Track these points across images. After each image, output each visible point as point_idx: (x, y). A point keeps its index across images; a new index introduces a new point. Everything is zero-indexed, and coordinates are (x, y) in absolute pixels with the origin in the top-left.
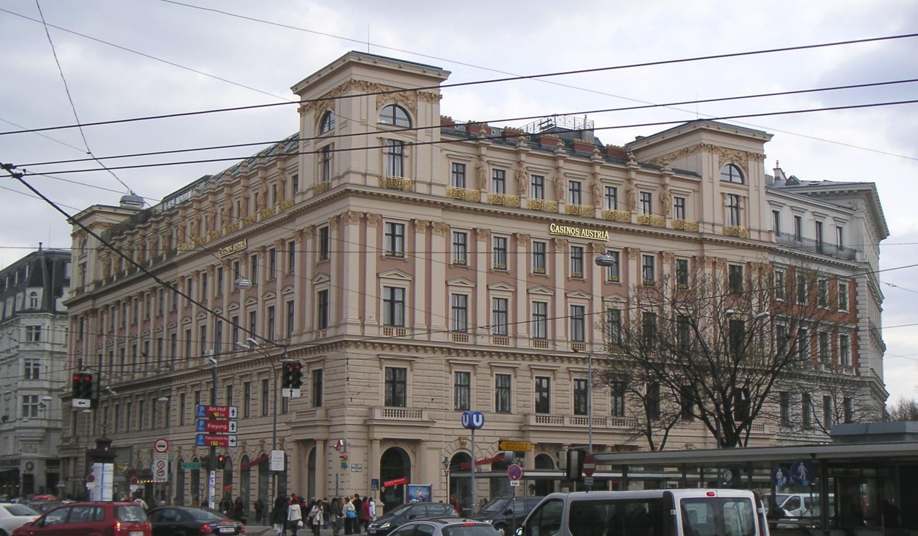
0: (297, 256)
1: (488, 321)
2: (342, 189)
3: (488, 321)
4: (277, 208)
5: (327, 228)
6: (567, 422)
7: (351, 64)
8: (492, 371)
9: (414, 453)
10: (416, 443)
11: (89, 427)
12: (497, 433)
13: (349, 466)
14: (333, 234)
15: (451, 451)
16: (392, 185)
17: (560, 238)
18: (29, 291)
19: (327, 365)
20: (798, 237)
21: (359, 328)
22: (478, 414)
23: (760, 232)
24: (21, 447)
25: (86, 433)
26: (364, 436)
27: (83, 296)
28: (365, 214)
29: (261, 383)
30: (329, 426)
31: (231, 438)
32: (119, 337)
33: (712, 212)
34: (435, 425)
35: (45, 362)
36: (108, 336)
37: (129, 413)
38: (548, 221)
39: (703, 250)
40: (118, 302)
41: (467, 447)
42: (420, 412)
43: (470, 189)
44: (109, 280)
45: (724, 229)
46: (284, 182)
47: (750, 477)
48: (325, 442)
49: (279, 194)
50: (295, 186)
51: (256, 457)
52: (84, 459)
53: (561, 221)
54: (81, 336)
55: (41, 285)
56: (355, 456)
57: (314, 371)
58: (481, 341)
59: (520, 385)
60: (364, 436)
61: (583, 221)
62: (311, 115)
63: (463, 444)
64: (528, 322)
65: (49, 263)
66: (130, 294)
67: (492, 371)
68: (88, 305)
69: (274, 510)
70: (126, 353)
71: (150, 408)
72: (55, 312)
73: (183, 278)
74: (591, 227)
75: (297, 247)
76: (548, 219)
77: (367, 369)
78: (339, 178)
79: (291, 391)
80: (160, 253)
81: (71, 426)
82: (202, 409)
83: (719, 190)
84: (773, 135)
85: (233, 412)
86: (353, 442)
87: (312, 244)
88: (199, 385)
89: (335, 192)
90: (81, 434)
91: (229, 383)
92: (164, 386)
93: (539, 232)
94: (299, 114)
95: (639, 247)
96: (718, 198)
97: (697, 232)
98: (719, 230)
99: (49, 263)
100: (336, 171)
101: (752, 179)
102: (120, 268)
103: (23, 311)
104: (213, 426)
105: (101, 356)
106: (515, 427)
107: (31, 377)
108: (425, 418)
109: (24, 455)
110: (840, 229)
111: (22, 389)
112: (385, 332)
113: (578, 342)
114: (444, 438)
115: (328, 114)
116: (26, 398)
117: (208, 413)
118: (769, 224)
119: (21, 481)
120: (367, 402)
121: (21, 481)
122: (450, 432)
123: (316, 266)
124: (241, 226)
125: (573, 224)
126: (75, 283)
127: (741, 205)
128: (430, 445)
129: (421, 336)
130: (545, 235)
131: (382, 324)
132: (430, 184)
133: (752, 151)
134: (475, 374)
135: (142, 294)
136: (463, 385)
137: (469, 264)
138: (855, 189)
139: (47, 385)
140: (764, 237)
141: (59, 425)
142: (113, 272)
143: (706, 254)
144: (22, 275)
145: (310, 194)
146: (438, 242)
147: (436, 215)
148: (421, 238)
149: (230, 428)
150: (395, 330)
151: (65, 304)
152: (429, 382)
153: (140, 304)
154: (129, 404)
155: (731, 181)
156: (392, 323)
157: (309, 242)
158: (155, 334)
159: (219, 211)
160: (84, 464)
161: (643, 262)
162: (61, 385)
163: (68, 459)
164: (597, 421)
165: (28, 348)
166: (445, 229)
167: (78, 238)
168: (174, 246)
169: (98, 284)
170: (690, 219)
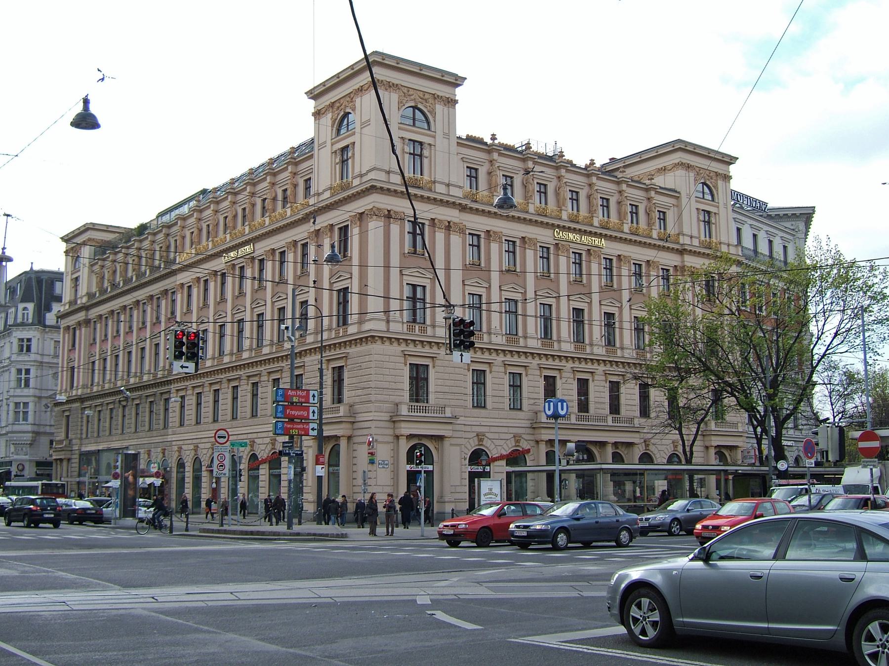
1: (536, 312)
3: (536, 312)
6: (573, 421)
10: (440, 438)
11: (82, 430)
13: (376, 462)
14: (354, 233)
15: (469, 447)
17: (563, 243)
18: (21, 306)
19: (349, 362)
20: (755, 251)
21: (384, 323)
22: (562, 401)
23: (729, 245)
24: (12, 449)
26: (390, 432)
27: (77, 307)
29: (230, 390)
37: (124, 416)
39: (683, 261)
41: (484, 443)
42: (443, 409)
44: (103, 291)
46: (295, 186)
49: (249, 216)
50: (307, 188)
51: (265, 456)
52: (77, 460)
53: (564, 227)
56: (383, 452)
59: (532, 384)
60: (390, 432)
61: (583, 228)
62: (327, 119)
66: (139, 298)
68: (81, 316)
70: (97, 367)
71: (147, 410)
72: (45, 326)
74: (590, 233)
76: (553, 224)
77: (391, 365)
78: (361, 176)
79: (462, 355)
80: (143, 268)
81: (63, 430)
82: (280, 392)
86: (380, 439)
90: (73, 436)
91: (216, 387)
92: (164, 389)
93: (545, 236)
95: (630, 254)
96: (694, 212)
97: (678, 243)
101: (721, 196)
103: (16, 325)
104: (293, 413)
105: (94, 363)
106: (527, 423)
108: (448, 414)
109: (16, 457)
116: (17, 404)
117: (286, 398)
120: (392, 398)
122: (190, 442)
124: (210, 247)
125: (574, 230)
126: (67, 298)
127: (713, 220)
128: (453, 441)
131: (405, 321)
132: (448, 185)
136: (479, 379)
137: (483, 265)
138: (798, 212)
143: (686, 263)
147: (453, 215)
149: (311, 415)
150: (417, 327)
153: (98, 326)
156: (414, 321)
159: (158, 249)
160: (77, 465)
163: (61, 460)
165: (20, 358)
169: (90, 295)
170: (671, 229)
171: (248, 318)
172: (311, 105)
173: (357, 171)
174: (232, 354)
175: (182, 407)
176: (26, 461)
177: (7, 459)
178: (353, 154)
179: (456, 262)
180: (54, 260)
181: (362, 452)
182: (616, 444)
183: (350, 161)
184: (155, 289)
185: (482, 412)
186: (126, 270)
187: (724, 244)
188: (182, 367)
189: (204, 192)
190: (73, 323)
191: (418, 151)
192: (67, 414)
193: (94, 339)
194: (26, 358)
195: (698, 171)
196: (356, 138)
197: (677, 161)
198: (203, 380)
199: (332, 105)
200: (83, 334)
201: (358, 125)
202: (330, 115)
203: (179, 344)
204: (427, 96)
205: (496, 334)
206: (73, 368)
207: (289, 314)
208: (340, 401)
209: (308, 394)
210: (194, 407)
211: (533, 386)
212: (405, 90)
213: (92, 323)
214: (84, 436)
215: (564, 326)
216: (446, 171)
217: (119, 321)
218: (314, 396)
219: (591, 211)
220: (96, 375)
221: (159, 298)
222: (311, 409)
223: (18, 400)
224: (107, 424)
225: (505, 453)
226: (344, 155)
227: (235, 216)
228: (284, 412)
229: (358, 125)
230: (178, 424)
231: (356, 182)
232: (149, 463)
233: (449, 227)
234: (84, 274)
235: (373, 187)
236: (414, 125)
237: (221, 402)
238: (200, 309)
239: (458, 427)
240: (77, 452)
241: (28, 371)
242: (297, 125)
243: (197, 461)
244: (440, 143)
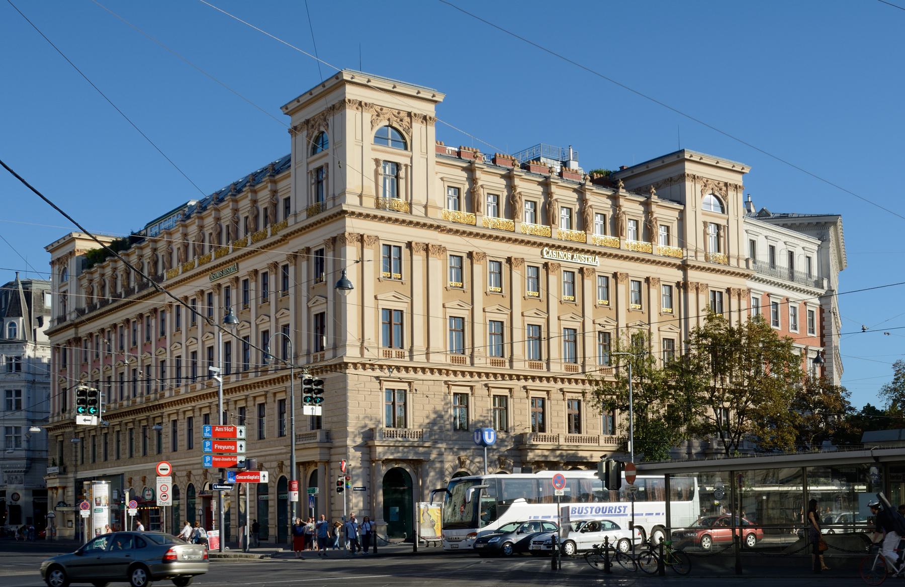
11: (76, 456)
14: (329, 257)
25: (74, 463)
27: (65, 324)
37: (118, 441)
40: (103, 330)
44: (92, 308)
47: (805, 488)
49: (270, 217)
50: (287, 208)
54: (65, 366)
62: (302, 136)
68: (70, 334)
69: (565, 570)
71: (141, 435)
87: (305, 268)
92: (156, 413)
94: (289, 135)
104: (220, 447)
107: (13, 407)
110: (809, 258)
119: (8, 513)
121: (8, 513)
129: (420, 359)
135: (115, 326)
151: (46, 333)
157: (304, 264)
164: (590, 440)
167: (57, 267)
168: (160, 273)
171: (154, 364)
172: (49, 257)
175: (175, 432)
178: (327, 176)
183: (324, 182)
193: (86, 360)
194: (16, 377)
199: (307, 122)
202: (305, 133)
206: (65, 390)
213: (83, 342)
214: (79, 462)
221: (148, 317)
222: (239, 443)
224: (102, 450)
237: (194, 430)
240: (72, 480)
243: (191, 488)
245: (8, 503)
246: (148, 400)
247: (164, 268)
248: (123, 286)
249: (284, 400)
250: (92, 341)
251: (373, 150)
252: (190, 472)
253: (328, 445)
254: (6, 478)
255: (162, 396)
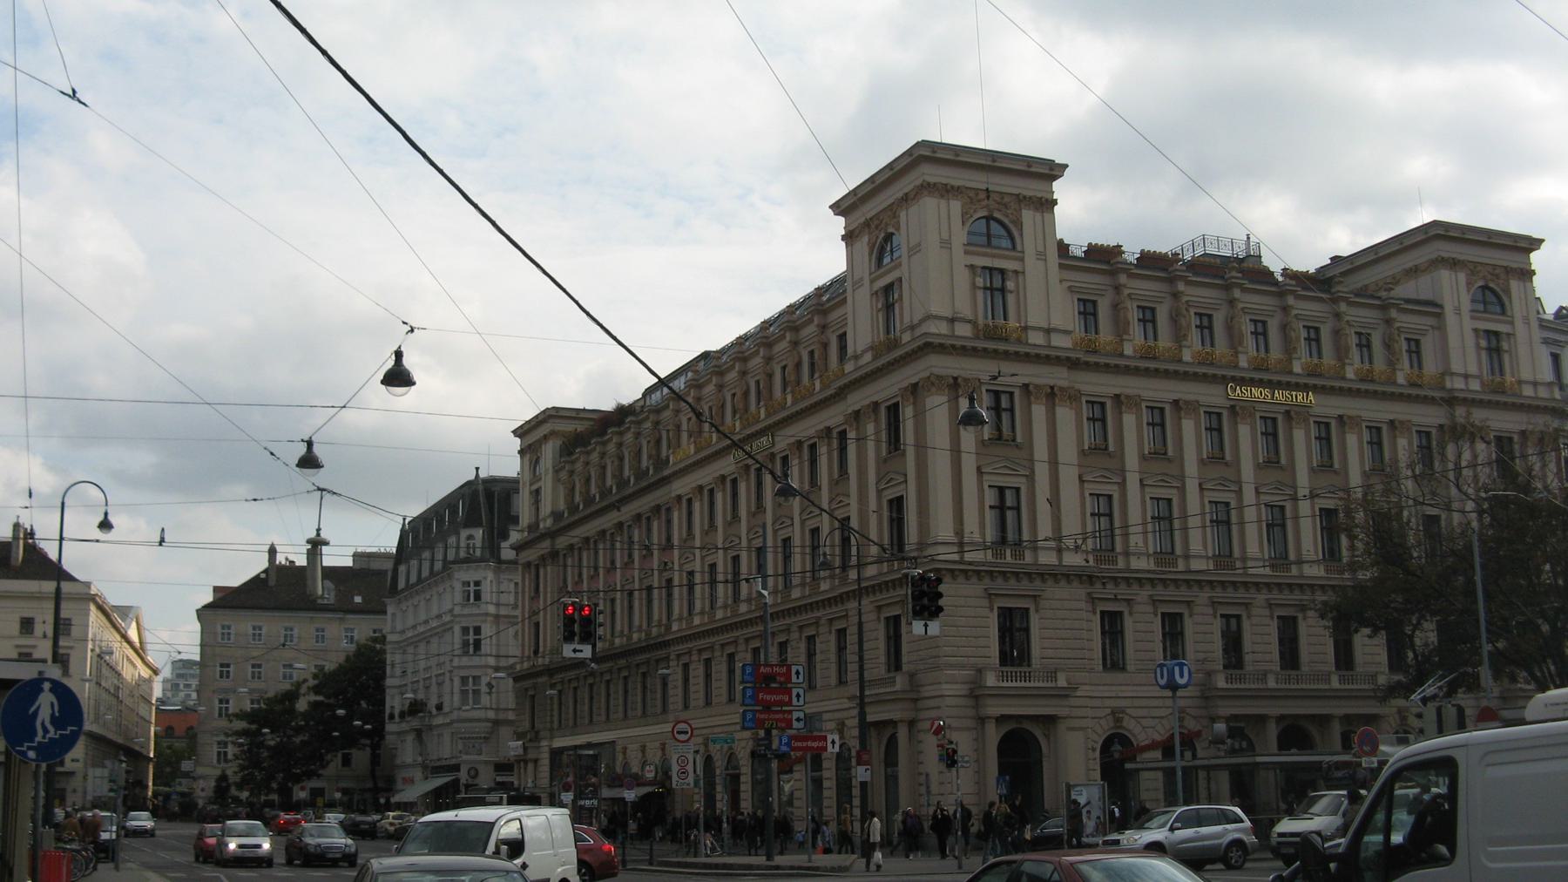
0: (852, 449)
2: (920, 343)
4: (763, 411)
5: (896, 405)
6: (1272, 684)
7: (551, 416)
8: (1156, 608)
9: (1047, 736)
10: (1050, 721)
12: (1108, 703)
14: (908, 412)
15: (1100, 731)
16: (992, 334)
18: (464, 533)
26: (971, 712)
28: (955, 379)
30: (916, 700)
31: (795, 715)
32: (641, 569)
33: (1462, 355)
34: (1079, 693)
35: (487, 630)
36: (680, 548)
37: (608, 695)
38: (1224, 380)
42: (1052, 675)
43: (1106, 335)
44: (573, 509)
45: (1482, 384)
46: (825, 346)
48: (912, 723)
49: (764, 392)
50: (843, 348)
55: (480, 525)
57: (887, 619)
58: (1136, 563)
60: (971, 712)
61: (1275, 378)
62: (863, 243)
63: (1118, 720)
64: (1204, 527)
65: (489, 495)
67: (1156, 608)
72: (500, 561)
73: (679, 498)
74: (1288, 386)
75: (851, 435)
76: (1224, 377)
78: (912, 328)
81: (527, 717)
83: (1468, 325)
84: (1542, 241)
85: (798, 673)
86: (954, 723)
88: (711, 648)
89: (908, 349)
91: (730, 650)
92: (661, 653)
93: (1210, 396)
98: (1475, 385)
99: (489, 495)
100: (907, 320)
102: (588, 491)
109: (465, 757)
111: (459, 667)
112: (995, 555)
113: (1280, 560)
114: (1090, 713)
115: (889, 237)
116: (464, 680)
118: (1547, 375)
122: (1097, 703)
123: (882, 462)
125: (1260, 383)
126: (525, 518)
129: (1047, 558)
130: (1220, 401)
133: (1515, 265)
134: (1131, 614)
135: (603, 532)
136: (1112, 626)
139: (492, 661)
140: (1543, 393)
141: (511, 716)
142: (577, 498)
144: (454, 512)
145: (868, 357)
146: (1065, 414)
147: (1058, 377)
148: (1039, 411)
150: (1008, 552)
151: (512, 547)
152: (1063, 628)
154: (608, 682)
155: (1485, 311)
157: (870, 428)
158: (749, 541)
159: (729, 398)
161: (1366, 437)
162: (512, 661)
165: (466, 611)
166: (1073, 396)
169: (557, 516)
170: (1431, 366)
171: (698, 568)
173: (907, 320)
174: (725, 607)
176: (480, 762)
177: (454, 762)
178: (901, 296)
179: (1068, 452)
180: (506, 462)
181: (930, 746)
182: (1347, 719)
183: (897, 306)
184: (643, 504)
185: (1119, 677)
186: (621, 468)
187: (1527, 382)
188: (575, 651)
189: (706, 356)
190: (708, 479)
191: (996, 285)
192: (531, 693)
195: (1472, 268)
196: (902, 272)
197: (1434, 256)
198: (788, 621)
199: (867, 224)
200: (549, 573)
201: (904, 250)
202: (866, 239)
203: (569, 621)
204: (1007, 199)
205: (1138, 555)
207: (720, 568)
208: (898, 668)
209: (789, 670)
210: (701, 680)
211: (1204, 636)
212: (972, 194)
214: (556, 725)
215: (1252, 531)
216: (1046, 308)
217: (613, 548)
218: (798, 673)
219: (1289, 350)
220: (676, 604)
222: (794, 692)
223: (464, 673)
224: (586, 708)
225: (1158, 738)
226: (888, 297)
227: (798, 365)
228: (754, 697)
229: (904, 250)
230: (680, 706)
231: (906, 337)
232: (644, 764)
233: (1052, 395)
234: (547, 485)
235: (928, 345)
236: (989, 244)
238: (705, 533)
239: (1072, 701)
241: (477, 630)
242: (821, 256)
244: (1032, 266)
245: (463, 781)
246: (648, 634)
247: (669, 447)
248: (614, 476)
249: (845, 630)
250: (748, 480)
251: (966, 252)
252: (843, 724)
253: (914, 696)
254: (460, 747)
255: (668, 627)
